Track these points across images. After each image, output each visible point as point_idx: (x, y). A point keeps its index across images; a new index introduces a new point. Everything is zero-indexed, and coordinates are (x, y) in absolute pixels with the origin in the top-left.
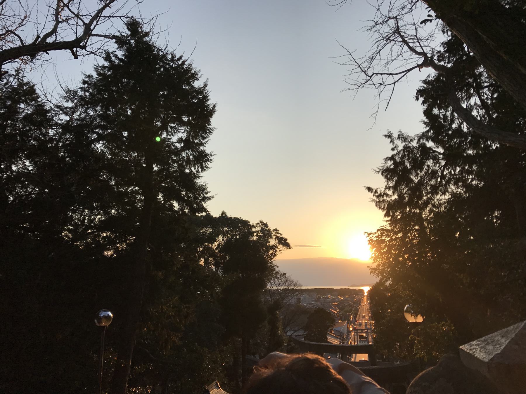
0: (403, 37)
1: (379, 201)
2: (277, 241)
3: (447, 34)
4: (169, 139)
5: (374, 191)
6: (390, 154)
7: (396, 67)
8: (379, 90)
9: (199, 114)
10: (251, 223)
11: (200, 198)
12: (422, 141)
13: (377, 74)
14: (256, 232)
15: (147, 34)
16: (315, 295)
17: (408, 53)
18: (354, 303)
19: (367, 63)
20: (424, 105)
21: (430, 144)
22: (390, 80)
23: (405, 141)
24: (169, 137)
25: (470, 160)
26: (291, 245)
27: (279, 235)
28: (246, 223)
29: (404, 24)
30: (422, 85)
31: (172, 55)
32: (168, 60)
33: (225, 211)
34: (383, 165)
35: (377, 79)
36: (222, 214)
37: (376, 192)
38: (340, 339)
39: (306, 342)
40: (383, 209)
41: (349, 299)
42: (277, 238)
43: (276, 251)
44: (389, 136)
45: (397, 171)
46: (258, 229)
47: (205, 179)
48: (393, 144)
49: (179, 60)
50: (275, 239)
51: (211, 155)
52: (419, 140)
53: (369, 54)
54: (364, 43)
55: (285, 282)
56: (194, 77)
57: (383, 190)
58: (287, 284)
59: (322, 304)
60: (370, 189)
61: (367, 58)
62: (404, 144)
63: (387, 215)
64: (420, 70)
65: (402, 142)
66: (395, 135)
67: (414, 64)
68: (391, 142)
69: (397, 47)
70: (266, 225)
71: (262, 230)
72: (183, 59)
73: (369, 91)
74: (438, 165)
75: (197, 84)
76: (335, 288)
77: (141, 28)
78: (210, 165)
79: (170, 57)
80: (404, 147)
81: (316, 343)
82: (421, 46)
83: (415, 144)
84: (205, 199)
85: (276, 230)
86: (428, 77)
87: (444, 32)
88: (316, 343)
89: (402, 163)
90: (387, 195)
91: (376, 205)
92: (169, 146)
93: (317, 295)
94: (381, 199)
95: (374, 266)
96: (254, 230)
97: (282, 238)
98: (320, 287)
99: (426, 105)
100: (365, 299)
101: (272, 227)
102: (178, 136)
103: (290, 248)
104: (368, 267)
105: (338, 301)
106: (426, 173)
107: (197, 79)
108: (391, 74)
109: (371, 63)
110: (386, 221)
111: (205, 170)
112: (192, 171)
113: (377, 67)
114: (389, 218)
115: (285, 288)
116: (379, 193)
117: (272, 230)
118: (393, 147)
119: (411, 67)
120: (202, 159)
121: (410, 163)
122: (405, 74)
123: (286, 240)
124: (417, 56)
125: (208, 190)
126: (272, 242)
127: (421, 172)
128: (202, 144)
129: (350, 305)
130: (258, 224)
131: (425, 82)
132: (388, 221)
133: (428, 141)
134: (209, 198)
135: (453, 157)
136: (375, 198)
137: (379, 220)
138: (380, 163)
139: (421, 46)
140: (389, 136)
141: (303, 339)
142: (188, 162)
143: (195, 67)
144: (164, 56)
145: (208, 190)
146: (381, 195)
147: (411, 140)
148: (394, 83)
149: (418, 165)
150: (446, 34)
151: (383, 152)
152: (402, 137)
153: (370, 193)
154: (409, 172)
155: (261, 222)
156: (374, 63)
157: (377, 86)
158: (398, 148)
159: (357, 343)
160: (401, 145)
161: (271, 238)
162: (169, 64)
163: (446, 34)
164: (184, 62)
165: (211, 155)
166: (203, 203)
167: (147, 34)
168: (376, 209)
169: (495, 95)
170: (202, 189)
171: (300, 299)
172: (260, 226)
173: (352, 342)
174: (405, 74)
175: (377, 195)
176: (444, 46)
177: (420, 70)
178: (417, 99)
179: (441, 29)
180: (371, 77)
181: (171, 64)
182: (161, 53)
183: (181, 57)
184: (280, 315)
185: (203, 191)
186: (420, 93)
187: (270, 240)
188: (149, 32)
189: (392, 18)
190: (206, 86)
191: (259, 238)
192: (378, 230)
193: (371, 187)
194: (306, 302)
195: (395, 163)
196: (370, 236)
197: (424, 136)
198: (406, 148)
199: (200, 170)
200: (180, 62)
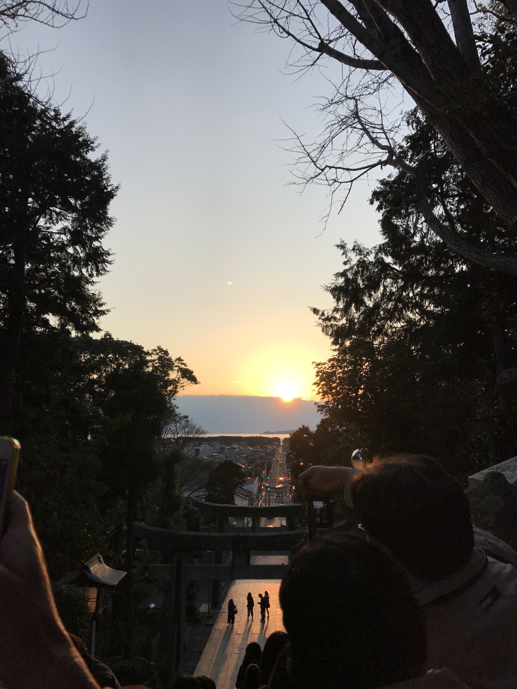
0: (362, 125)
1: (327, 326)
2: (180, 374)
3: (412, 126)
4: (48, 228)
5: (320, 313)
6: (342, 268)
7: (354, 160)
8: (333, 188)
9: (92, 196)
10: (145, 350)
11: (91, 312)
12: (380, 255)
13: (330, 167)
14: (151, 361)
15: (19, 77)
16: (218, 446)
17: (370, 146)
18: (267, 454)
19: (316, 152)
20: (379, 211)
21: (389, 260)
22: (346, 176)
23: (360, 254)
24: (48, 225)
25: (430, 282)
26: (198, 380)
27: (183, 366)
28: (138, 350)
29: (363, 107)
30: (379, 186)
31: (55, 110)
32: (48, 118)
33: (110, 332)
34: (333, 282)
35: (331, 174)
36: (105, 336)
37: (323, 314)
38: (249, 500)
39: (208, 503)
40: (331, 335)
41: (261, 450)
42: (181, 369)
43: (176, 387)
44: (342, 247)
45: (348, 291)
46: (155, 357)
47: (100, 286)
48: (346, 257)
49: (64, 119)
50: (178, 371)
51: (109, 254)
52: (377, 254)
53: (320, 141)
54: (315, 127)
55: (184, 427)
56: (87, 145)
57: (331, 313)
58: (187, 430)
59: (226, 457)
60: (315, 311)
61: (318, 146)
62: (358, 257)
63: (335, 343)
64: (382, 169)
65: (356, 255)
66: (350, 246)
67: (376, 161)
68: (343, 254)
69: (355, 135)
70: (166, 353)
71: (160, 358)
72: (71, 119)
73: (320, 189)
74: (395, 285)
75: (92, 156)
76: (244, 435)
77: (15, 67)
78: (109, 267)
79: (52, 113)
80: (359, 261)
81: (222, 505)
82: (387, 138)
83: (371, 258)
84: (98, 313)
85: (179, 359)
86: (389, 176)
87: (408, 123)
88: (222, 505)
89: (355, 281)
90: (335, 319)
91: (323, 331)
92: (47, 238)
93: (221, 445)
94: (329, 323)
95: (323, 402)
96: (148, 358)
97: (187, 370)
98: (225, 435)
99: (382, 212)
100: (280, 450)
101: (173, 356)
102: (57, 226)
103: (196, 383)
104: (316, 403)
105: (246, 453)
106: (383, 295)
107: (93, 149)
108: (348, 169)
109: (321, 152)
110: (333, 350)
111: (101, 274)
112: (82, 274)
113: (330, 158)
114: (337, 347)
115: (184, 436)
116: (326, 315)
117: (174, 359)
118: (346, 260)
119: (373, 163)
120: (97, 258)
121: (363, 281)
122: (366, 172)
123: (192, 372)
124: (380, 150)
125: (103, 301)
126: (173, 375)
127: (375, 292)
128: (97, 238)
129: (262, 458)
130: (155, 350)
131: (382, 182)
132: (335, 350)
133: (387, 256)
134: (103, 313)
135: (411, 276)
136: (321, 321)
137: (325, 350)
138: (331, 281)
139: (387, 138)
140: (342, 247)
141: (204, 500)
142: (76, 261)
143: (91, 132)
144: (44, 111)
145: (103, 301)
146: (328, 319)
147: (368, 254)
148: (352, 181)
149: (373, 284)
150: (410, 127)
151: (332, 267)
152: (358, 249)
153: (315, 315)
154: (362, 292)
155: (159, 348)
156: (325, 153)
157: (331, 182)
158: (352, 262)
159: (269, 505)
160: (355, 259)
161: (172, 369)
162: (50, 124)
163: (410, 127)
164: (72, 124)
165: (109, 254)
166: (95, 318)
167: (19, 77)
168: (323, 335)
169: (462, 207)
170: (94, 300)
171: (198, 450)
172: (157, 354)
173: (261, 504)
174: (366, 172)
175: (323, 318)
176: (407, 141)
177: (382, 169)
178: (372, 203)
179: (405, 119)
180: (323, 170)
181: (54, 123)
182: (39, 107)
183: (68, 116)
184: (178, 468)
185: (95, 302)
186: (376, 195)
187: (170, 372)
188: (23, 74)
189: (350, 98)
190: (104, 160)
191: (156, 369)
192: (330, 360)
193: (317, 308)
194: (206, 453)
195: (347, 280)
196: (319, 367)
197: (382, 249)
198: (361, 264)
199: (95, 273)
200: (66, 123)
